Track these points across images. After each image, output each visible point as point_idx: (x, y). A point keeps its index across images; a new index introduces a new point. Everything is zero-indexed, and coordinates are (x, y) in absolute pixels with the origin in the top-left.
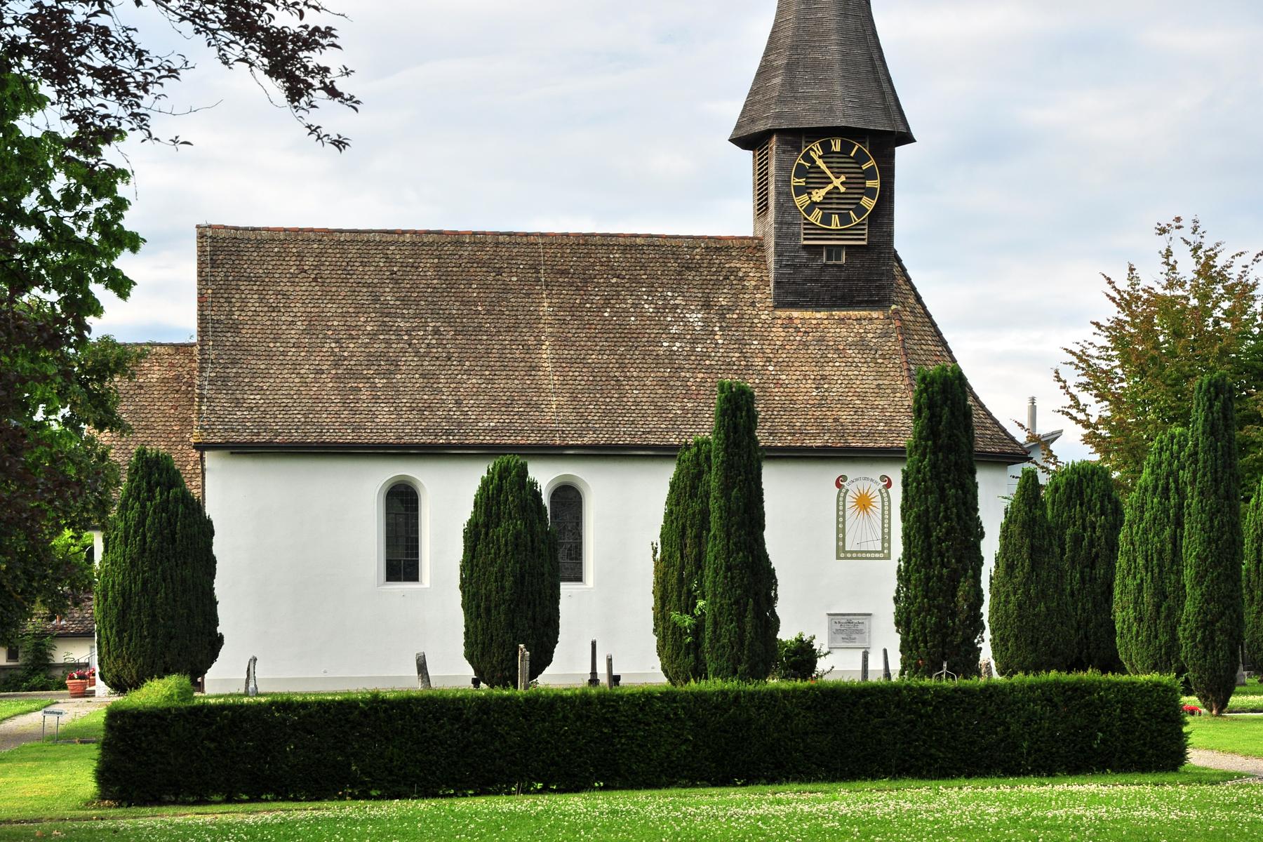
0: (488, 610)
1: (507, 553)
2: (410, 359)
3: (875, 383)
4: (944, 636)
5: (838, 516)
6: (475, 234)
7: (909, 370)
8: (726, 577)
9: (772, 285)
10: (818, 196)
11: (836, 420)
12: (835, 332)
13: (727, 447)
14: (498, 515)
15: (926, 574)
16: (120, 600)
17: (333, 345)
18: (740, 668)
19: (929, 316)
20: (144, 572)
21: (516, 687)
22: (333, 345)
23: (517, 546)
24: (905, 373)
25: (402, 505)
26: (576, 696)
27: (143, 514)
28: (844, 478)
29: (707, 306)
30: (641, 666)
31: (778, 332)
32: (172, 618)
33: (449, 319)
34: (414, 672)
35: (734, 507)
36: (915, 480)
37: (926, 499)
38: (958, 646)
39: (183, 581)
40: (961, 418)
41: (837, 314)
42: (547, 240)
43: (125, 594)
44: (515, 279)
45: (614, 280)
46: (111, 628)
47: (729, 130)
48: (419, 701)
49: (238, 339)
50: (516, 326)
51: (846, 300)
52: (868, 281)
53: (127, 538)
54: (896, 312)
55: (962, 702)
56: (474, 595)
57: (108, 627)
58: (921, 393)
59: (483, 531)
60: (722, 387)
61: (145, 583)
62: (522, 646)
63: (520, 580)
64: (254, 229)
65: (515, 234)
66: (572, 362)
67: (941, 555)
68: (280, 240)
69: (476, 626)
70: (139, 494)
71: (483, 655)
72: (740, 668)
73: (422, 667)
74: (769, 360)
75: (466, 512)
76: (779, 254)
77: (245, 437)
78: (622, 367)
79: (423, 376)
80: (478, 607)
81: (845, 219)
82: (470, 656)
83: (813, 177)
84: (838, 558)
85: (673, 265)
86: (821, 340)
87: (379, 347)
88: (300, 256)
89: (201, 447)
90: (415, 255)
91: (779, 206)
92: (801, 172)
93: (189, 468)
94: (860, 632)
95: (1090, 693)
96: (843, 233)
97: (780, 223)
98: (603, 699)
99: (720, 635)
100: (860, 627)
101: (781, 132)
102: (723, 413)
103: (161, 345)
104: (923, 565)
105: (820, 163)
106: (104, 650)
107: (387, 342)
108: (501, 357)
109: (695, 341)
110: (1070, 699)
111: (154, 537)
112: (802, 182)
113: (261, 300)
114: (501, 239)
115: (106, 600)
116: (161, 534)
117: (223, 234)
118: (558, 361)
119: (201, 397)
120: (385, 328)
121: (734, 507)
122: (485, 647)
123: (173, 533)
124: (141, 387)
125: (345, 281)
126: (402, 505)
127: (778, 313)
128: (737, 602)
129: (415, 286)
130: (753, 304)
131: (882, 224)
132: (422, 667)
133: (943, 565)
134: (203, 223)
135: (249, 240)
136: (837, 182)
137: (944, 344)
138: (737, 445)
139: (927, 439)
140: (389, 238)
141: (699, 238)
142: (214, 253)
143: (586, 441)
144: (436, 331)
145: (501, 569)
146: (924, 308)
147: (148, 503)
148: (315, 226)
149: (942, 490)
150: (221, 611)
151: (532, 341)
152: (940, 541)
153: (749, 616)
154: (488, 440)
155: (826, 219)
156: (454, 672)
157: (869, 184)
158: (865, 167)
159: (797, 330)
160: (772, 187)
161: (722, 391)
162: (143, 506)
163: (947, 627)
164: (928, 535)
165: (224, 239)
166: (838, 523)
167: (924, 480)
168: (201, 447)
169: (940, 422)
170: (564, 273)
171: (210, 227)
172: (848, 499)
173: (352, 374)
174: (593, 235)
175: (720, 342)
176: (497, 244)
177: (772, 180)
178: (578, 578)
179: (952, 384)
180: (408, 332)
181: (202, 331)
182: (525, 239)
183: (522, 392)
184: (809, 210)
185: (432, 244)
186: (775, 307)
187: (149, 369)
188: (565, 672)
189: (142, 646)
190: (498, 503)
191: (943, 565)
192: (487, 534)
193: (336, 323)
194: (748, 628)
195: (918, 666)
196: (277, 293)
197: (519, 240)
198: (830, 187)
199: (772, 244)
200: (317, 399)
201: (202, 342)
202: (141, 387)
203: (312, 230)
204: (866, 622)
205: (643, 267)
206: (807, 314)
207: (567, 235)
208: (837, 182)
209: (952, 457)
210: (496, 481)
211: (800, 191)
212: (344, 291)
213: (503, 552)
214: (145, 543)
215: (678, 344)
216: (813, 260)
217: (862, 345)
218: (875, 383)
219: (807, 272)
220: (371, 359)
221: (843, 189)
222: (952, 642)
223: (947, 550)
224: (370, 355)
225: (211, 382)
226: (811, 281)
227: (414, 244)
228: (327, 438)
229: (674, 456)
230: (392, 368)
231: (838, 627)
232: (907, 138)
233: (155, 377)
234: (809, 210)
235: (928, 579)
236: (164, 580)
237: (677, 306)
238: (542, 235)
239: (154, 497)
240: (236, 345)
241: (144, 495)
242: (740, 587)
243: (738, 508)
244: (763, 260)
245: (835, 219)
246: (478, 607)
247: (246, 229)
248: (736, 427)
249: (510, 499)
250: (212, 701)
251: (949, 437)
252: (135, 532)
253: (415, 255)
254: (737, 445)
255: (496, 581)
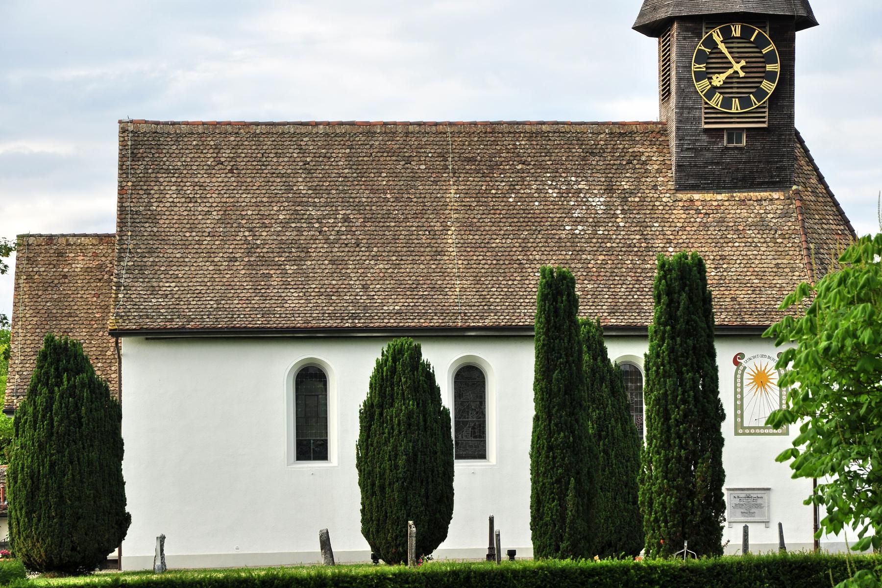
0: (382, 488)
1: (400, 432)
2: (321, 246)
3: (774, 262)
4: (684, 516)
5: (736, 393)
6: (385, 124)
7: (808, 249)
8: (547, 457)
9: (673, 168)
10: (718, 80)
11: (733, 299)
12: (736, 213)
13: (548, 330)
14: (392, 396)
15: (665, 456)
16: (29, 482)
17: (247, 234)
18: (563, 545)
19: (831, 196)
20: (52, 455)
21: (406, 564)
22: (247, 234)
23: (409, 425)
24: (804, 252)
25: (310, 384)
26: (311, 578)
27: (50, 400)
28: (742, 355)
29: (609, 190)
30: (520, 541)
31: (679, 214)
32: (79, 499)
33: (359, 207)
34: (317, 548)
35: (555, 389)
36: (655, 364)
37: (665, 382)
38: (698, 525)
39: (90, 462)
40: (700, 304)
41: (738, 195)
42: (456, 129)
43: (34, 477)
44: (423, 167)
45: (520, 167)
46: (21, 509)
47: (633, 19)
48: (482, 575)
49: (155, 229)
50: (423, 213)
51: (748, 182)
52: (769, 162)
53: (35, 422)
54: (797, 192)
55: (690, 580)
56: (369, 473)
57: (18, 507)
58: (660, 280)
59: (377, 411)
60: (543, 271)
61: (52, 465)
62: (411, 522)
63: (412, 460)
64: (173, 124)
65: (425, 124)
66: (476, 247)
67: (679, 437)
68: (198, 134)
69: (371, 504)
70: (48, 380)
71: (378, 531)
72: (563, 545)
73: (325, 542)
74: (669, 242)
75: (361, 393)
76: (680, 138)
77: (159, 323)
78: (525, 250)
79: (332, 262)
80: (373, 485)
81: (745, 102)
82: (366, 533)
83: (713, 60)
84: (737, 434)
85: (577, 150)
86: (722, 221)
87: (290, 235)
88: (217, 148)
89: (117, 334)
90: (328, 146)
91: (681, 92)
92: (701, 57)
93: (109, 353)
94: (759, 506)
95: (818, 572)
96: (743, 117)
97: (681, 108)
98: (502, 575)
99: (543, 513)
100: (759, 501)
101: (681, 19)
102: (544, 298)
103: (85, 236)
104: (662, 447)
105: (722, 47)
106: (15, 530)
107: (299, 230)
108: (408, 244)
109: (597, 224)
110: (798, 577)
111: (61, 422)
112: (702, 67)
113: (178, 191)
114: (411, 128)
115: (16, 482)
116: (68, 418)
117: (144, 128)
118: (463, 246)
119: (118, 285)
120: (296, 216)
121: (555, 389)
122: (377, 525)
123: (80, 418)
124: (65, 277)
125: (259, 172)
126: (310, 384)
127: (679, 196)
128: (558, 481)
129: (327, 175)
130: (655, 187)
131: (783, 107)
132: (325, 542)
133: (681, 447)
134: (126, 119)
135: (169, 134)
136: (737, 67)
137: (847, 222)
138: (558, 328)
139: (665, 324)
140: (303, 130)
141: (604, 124)
142: (135, 146)
143: (487, 322)
144: (346, 219)
145: (395, 448)
146: (826, 187)
147: (56, 389)
148: (232, 120)
149: (680, 373)
150: (455, 478)
151: (438, 227)
152: (678, 423)
153: (571, 494)
154: (392, 323)
155: (727, 103)
156: (354, 548)
157: (769, 67)
158: (765, 51)
159: (698, 211)
160: (673, 73)
161: (544, 277)
162: (52, 392)
163: (686, 507)
164: (666, 417)
165: (145, 133)
166: (736, 399)
167: (663, 365)
168: (117, 334)
169: (678, 307)
170: (470, 160)
171: (132, 122)
172: (746, 376)
173: (264, 261)
174: (500, 123)
175: (622, 224)
176: (407, 134)
177: (673, 66)
178: (480, 453)
179: (691, 270)
180: (319, 220)
181: (122, 223)
182: (434, 128)
183: (427, 276)
184: (710, 94)
185: (344, 135)
186: (677, 190)
187: (74, 259)
188: (461, 545)
189: (50, 526)
190: (392, 385)
191: (681, 447)
192: (381, 414)
193: (250, 213)
194: (570, 505)
195: (659, 546)
196: (195, 184)
197: (428, 129)
198: (730, 71)
199: (674, 128)
200: (229, 286)
201: (121, 232)
202: (65, 277)
203: (229, 123)
204: (765, 497)
205: (548, 153)
206: (708, 196)
207: (475, 124)
208: (737, 67)
209: (690, 342)
210: (389, 363)
211: (700, 76)
212: (259, 181)
213: (396, 432)
214: (53, 426)
215: (580, 228)
216: (714, 143)
217: (762, 225)
218: (774, 262)
219: (708, 155)
220: (283, 247)
221: (742, 74)
222: (691, 521)
223: (685, 432)
224: (282, 242)
225: (129, 270)
226: (712, 163)
227: (327, 135)
228: (237, 323)
229: (646, 336)
230: (303, 255)
231: (737, 501)
232: (809, 21)
233: (79, 266)
234: (710, 94)
235: (668, 460)
236: (71, 463)
237: (580, 191)
238: (451, 124)
239: (62, 383)
240: (153, 235)
241: (52, 380)
242: (561, 466)
243: (559, 391)
244: (666, 144)
245: (736, 102)
246: (373, 485)
247: (166, 123)
248: (556, 311)
249: (403, 380)
250: (129, 579)
251: (687, 323)
252: (44, 416)
253: (328, 146)
254: (558, 328)
255: (390, 460)
